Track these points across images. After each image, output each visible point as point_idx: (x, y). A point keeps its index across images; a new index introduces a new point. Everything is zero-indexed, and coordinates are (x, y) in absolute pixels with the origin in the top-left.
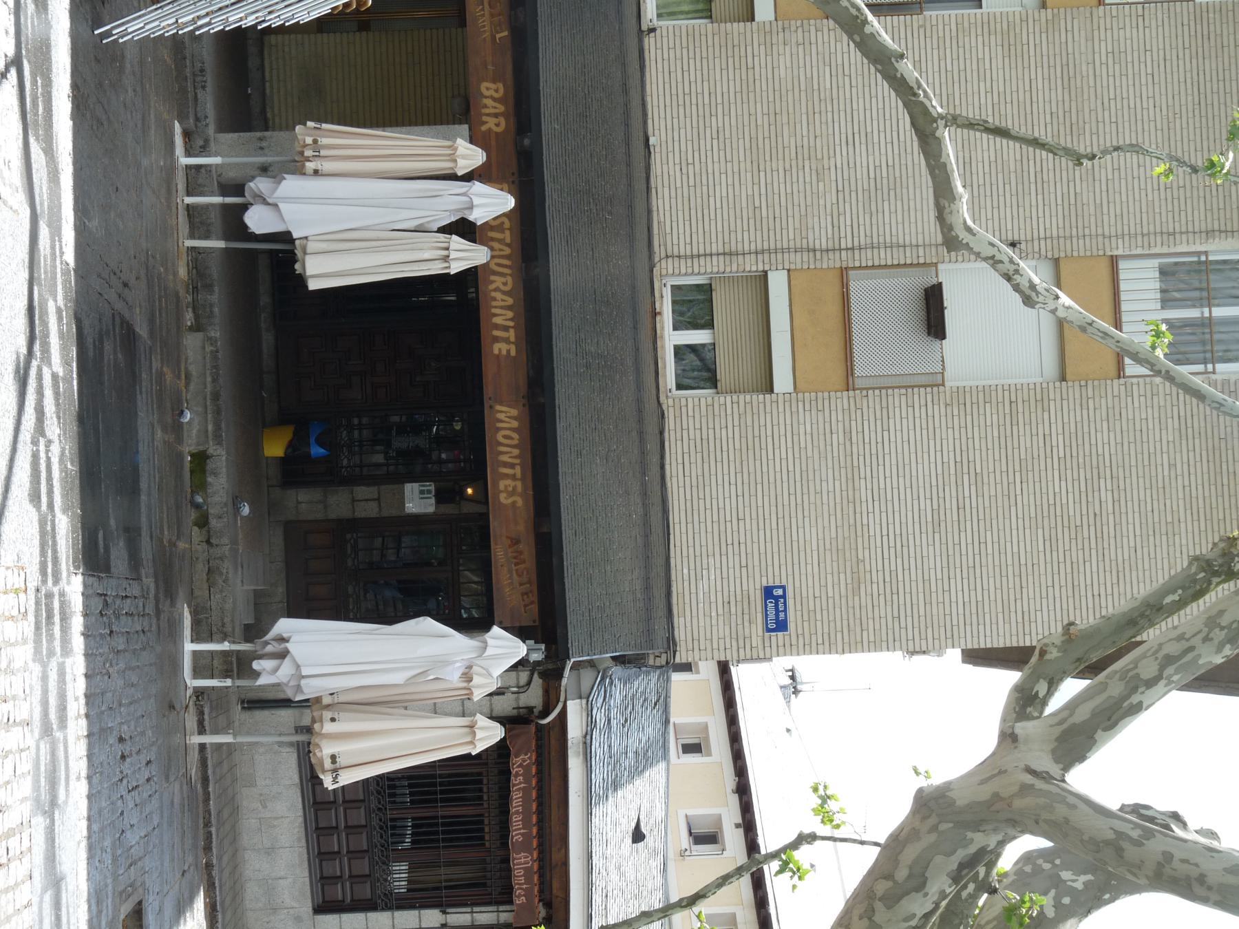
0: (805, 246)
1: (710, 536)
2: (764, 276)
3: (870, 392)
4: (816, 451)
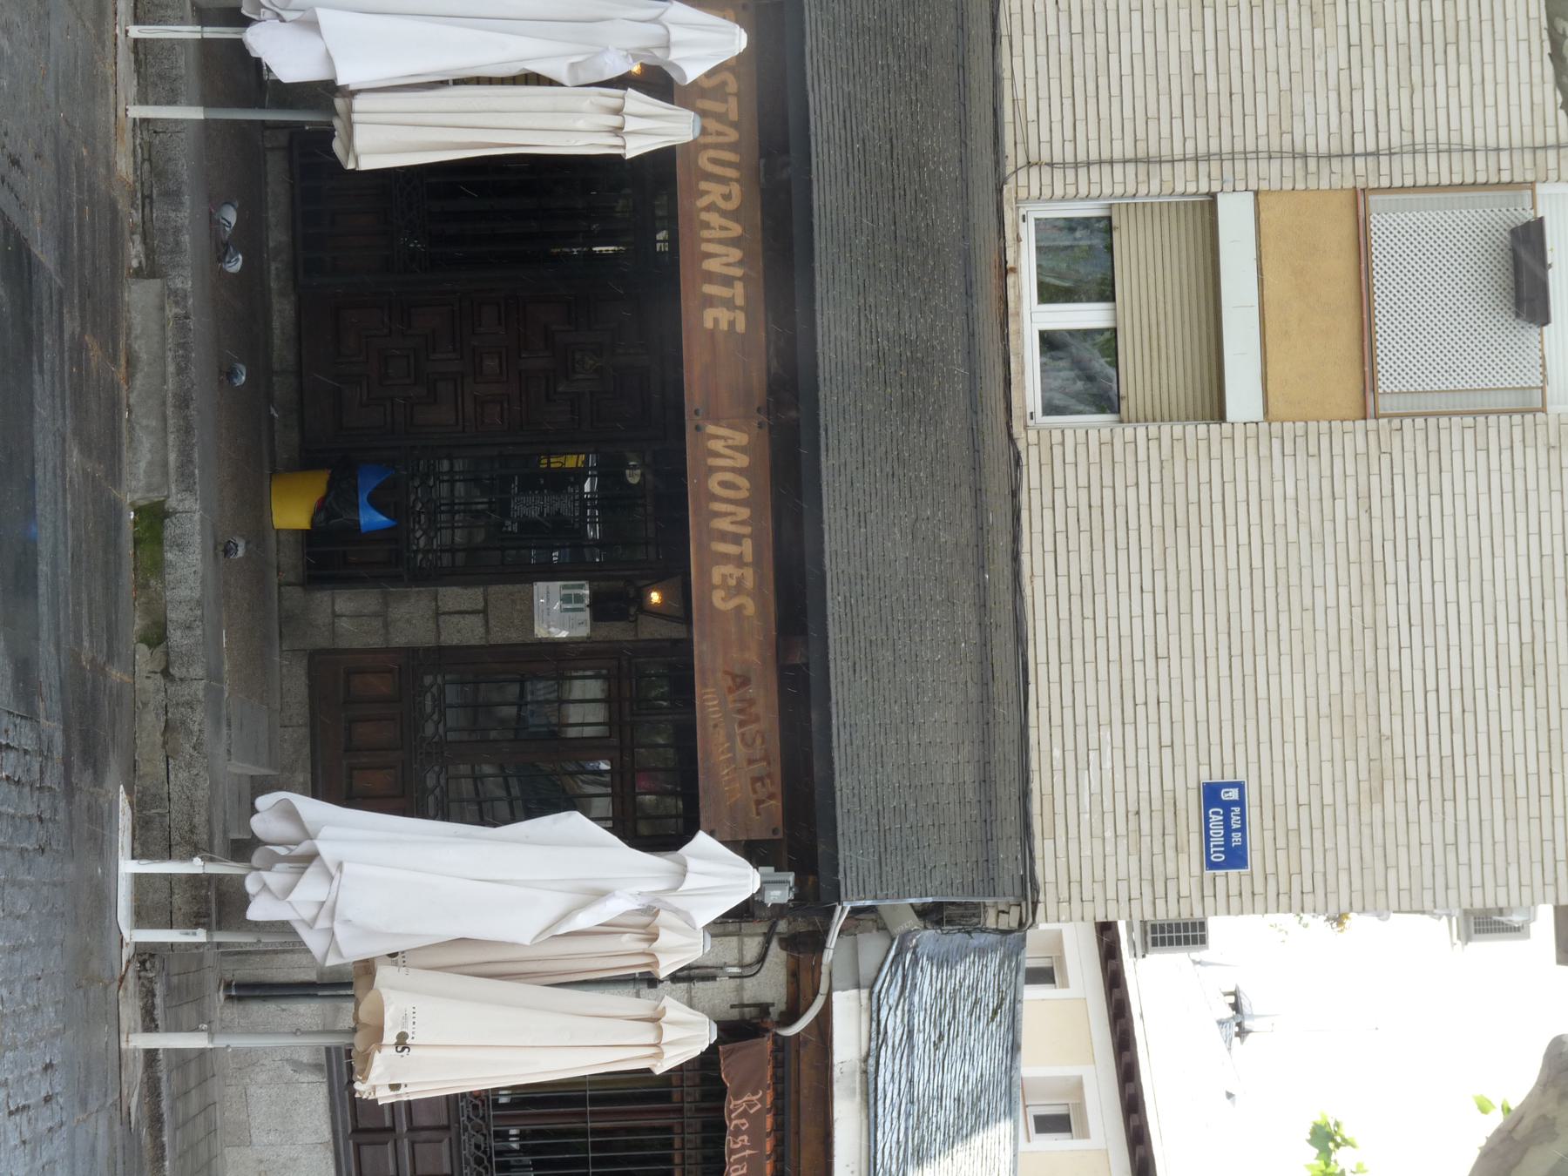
0: (1287, 147)
1: (1103, 686)
2: (1210, 203)
3: (1407, 422)
4: (1304, 529)
